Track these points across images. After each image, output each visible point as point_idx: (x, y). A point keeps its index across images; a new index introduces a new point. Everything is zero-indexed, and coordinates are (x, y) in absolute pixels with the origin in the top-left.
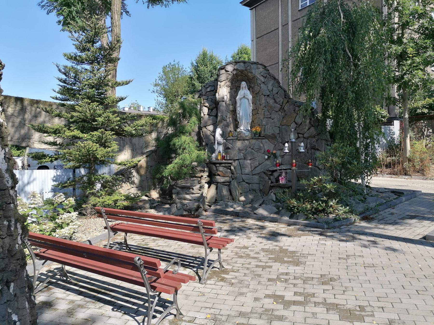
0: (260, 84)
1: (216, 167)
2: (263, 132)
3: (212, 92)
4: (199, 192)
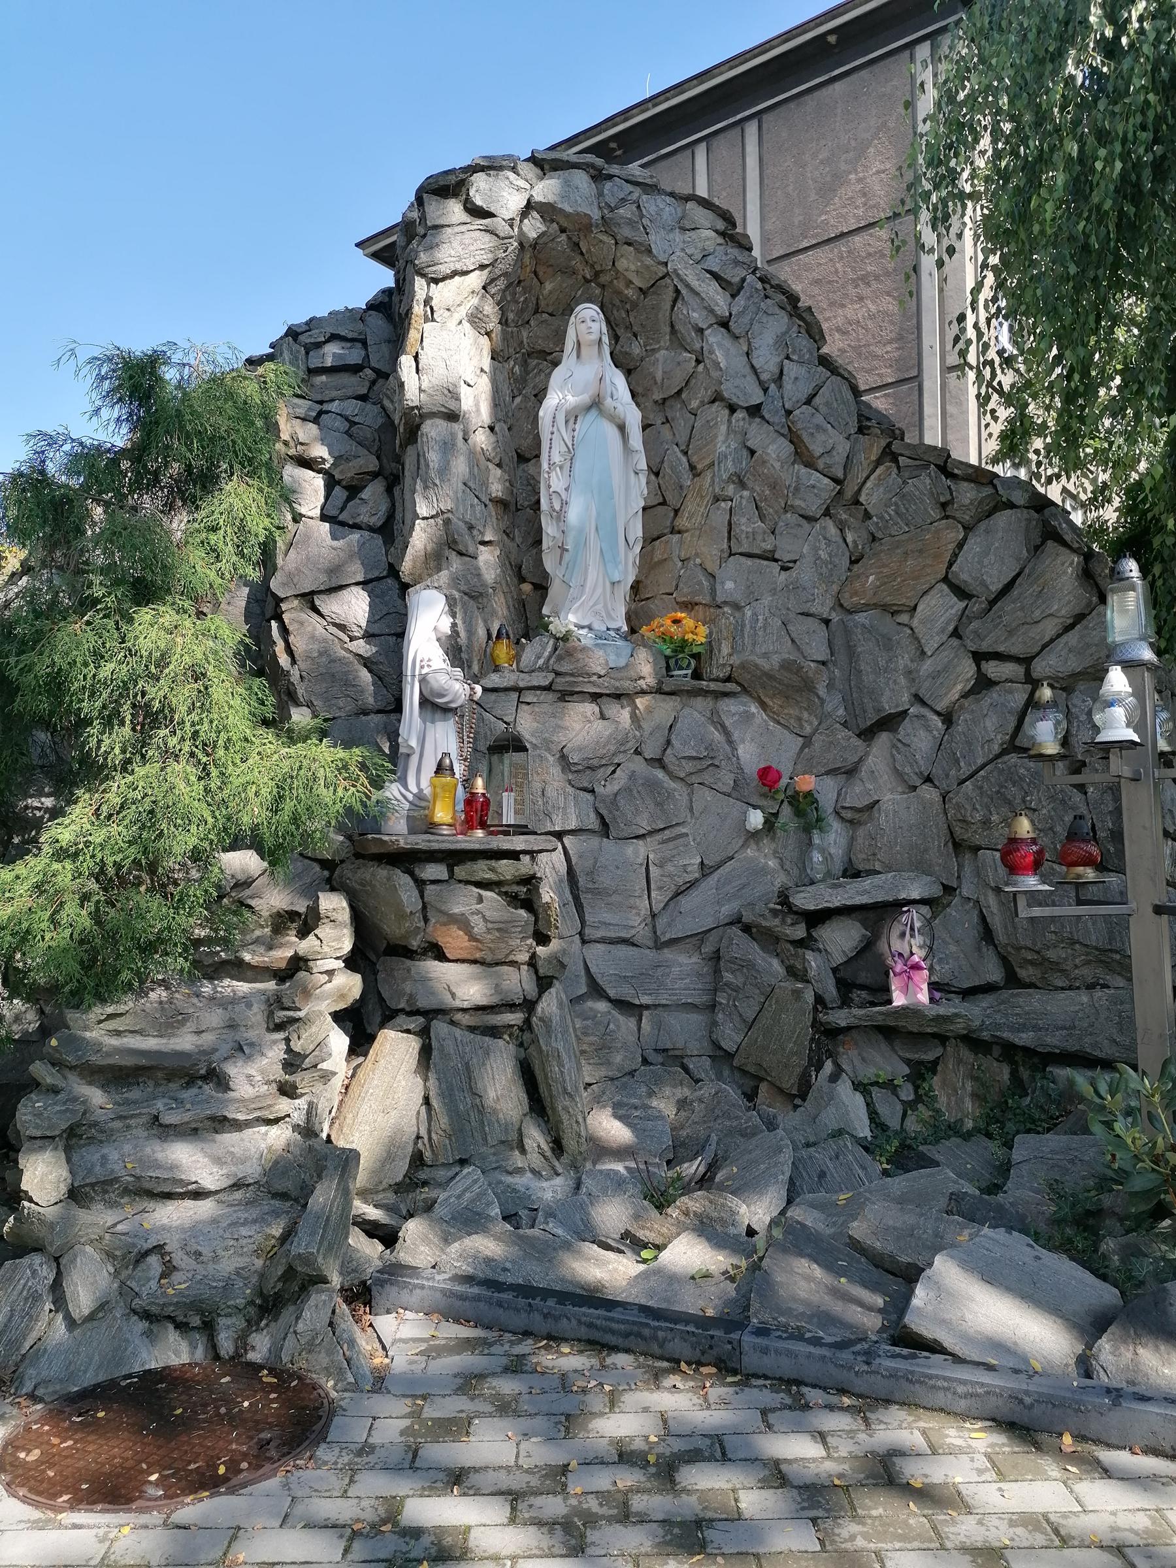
0: (701, 331)
1: (420, 884)
2: (725, 649)
3: (346, 379)
4: (284, 1105)
